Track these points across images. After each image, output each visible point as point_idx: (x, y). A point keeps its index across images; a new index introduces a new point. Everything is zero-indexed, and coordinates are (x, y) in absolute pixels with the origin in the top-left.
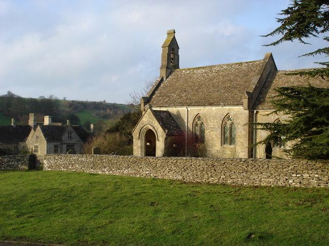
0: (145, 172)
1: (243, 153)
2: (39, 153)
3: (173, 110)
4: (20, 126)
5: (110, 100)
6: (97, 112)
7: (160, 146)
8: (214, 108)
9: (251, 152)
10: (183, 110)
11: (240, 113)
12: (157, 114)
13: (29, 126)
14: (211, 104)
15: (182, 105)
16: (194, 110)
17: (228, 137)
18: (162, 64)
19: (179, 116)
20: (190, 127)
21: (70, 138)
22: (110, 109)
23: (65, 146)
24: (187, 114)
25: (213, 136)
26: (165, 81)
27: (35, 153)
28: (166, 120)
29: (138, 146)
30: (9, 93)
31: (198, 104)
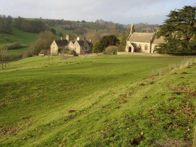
0: (59, 60)
1: (149, 52)
2: (77, 50)
3: (134, 43)
4: (64, 40)
5: (66, 18)
6: (61, 26)
7: (132, 50)
8: (144, 43)
9: (150, 52)
10: (137, 43)
11: (149, 44)
12: (131, 43)
13: (66, 40)
14: (143, 42)
15: (136, 41)
16: (139, 43)
17: (146, 48)
18: (124, 25)
19: (136, 44)
20: (138, 45)
21: (86, 45)
22: (68, 24)
23: (84, 48)
24: (138, 44)
25: (143, 48)
26: (132, 35)
27: (75, 50)
28: (133, 44)
29: (127, 50)
30: (19, 17)
31: (140, 42)
